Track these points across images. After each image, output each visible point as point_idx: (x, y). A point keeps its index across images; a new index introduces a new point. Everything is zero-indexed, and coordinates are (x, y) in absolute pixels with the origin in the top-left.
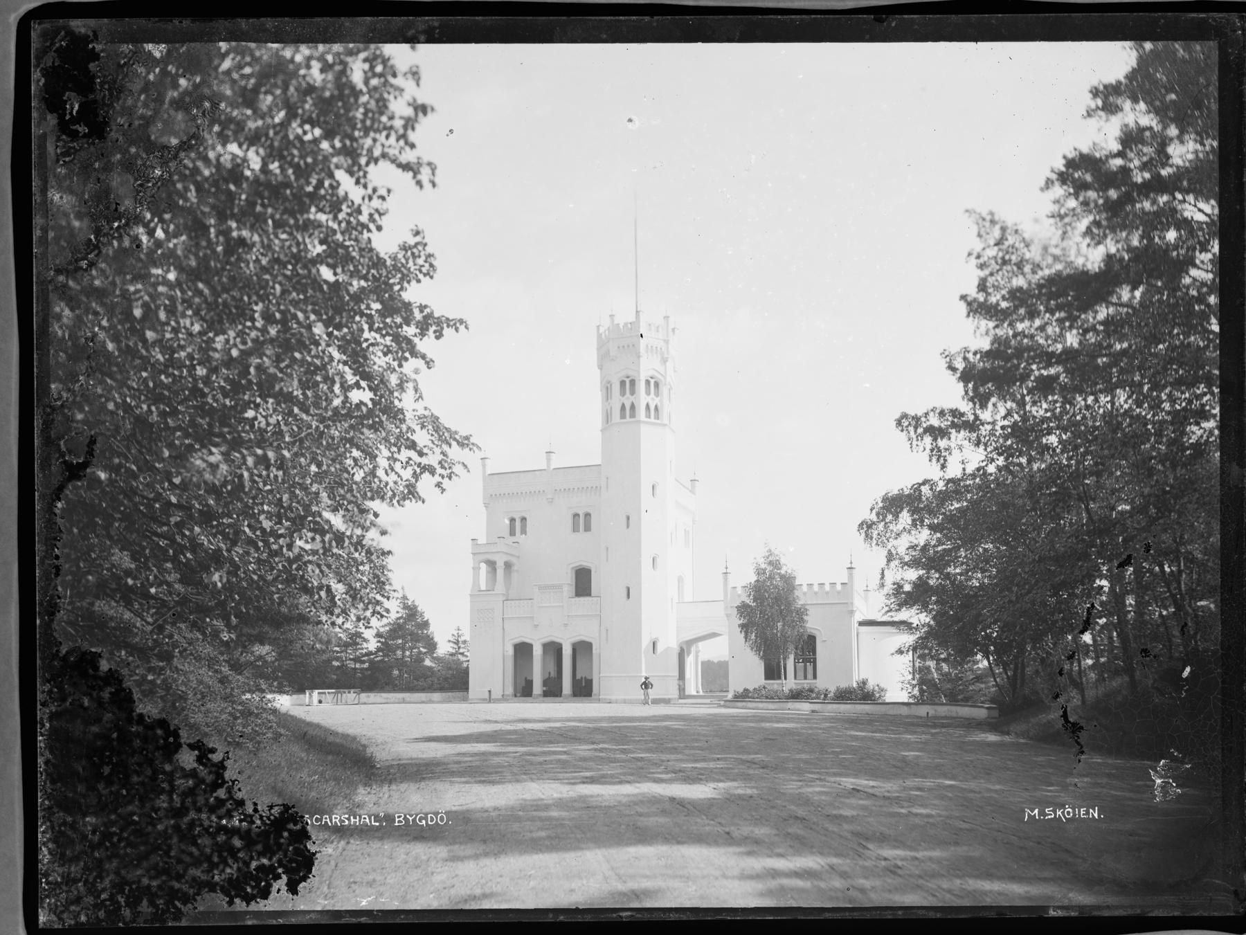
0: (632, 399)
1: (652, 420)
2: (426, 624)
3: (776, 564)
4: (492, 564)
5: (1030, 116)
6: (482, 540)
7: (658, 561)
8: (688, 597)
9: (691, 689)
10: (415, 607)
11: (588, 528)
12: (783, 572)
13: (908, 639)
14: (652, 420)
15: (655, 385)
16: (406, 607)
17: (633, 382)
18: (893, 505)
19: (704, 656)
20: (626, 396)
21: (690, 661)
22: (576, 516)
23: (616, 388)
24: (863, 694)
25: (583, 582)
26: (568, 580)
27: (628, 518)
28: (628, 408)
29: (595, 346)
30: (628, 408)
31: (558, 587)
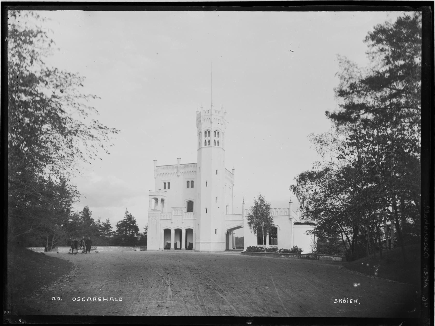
0: (209, 138)
1: (216, 146)
2: (135, 222)
3: (262, 201)
4: (156, 200)
5: (352, 42)
6: (153, 190)
7: (218, 172)
8: (230, 213)
9: (231, 248)
10: (131, 216)
11: (192, 186)
12: (265, 203)
13: (312, 228)
14: (216, 146)
15: (217, 133)
16: (128, 215)
17: (209, 132)
18: (304, 177)
19: (235, 236)
20: (208, 137)
21: (231, 237)
22: (188, 182)
23: (203, 134)
24: (296, 251)
25: (190, 206)
26: (185, 206)
27: (207, 182)
28: (207, 141)
29: (196, 119)
30: (207, 141)
31: (180, 209)
